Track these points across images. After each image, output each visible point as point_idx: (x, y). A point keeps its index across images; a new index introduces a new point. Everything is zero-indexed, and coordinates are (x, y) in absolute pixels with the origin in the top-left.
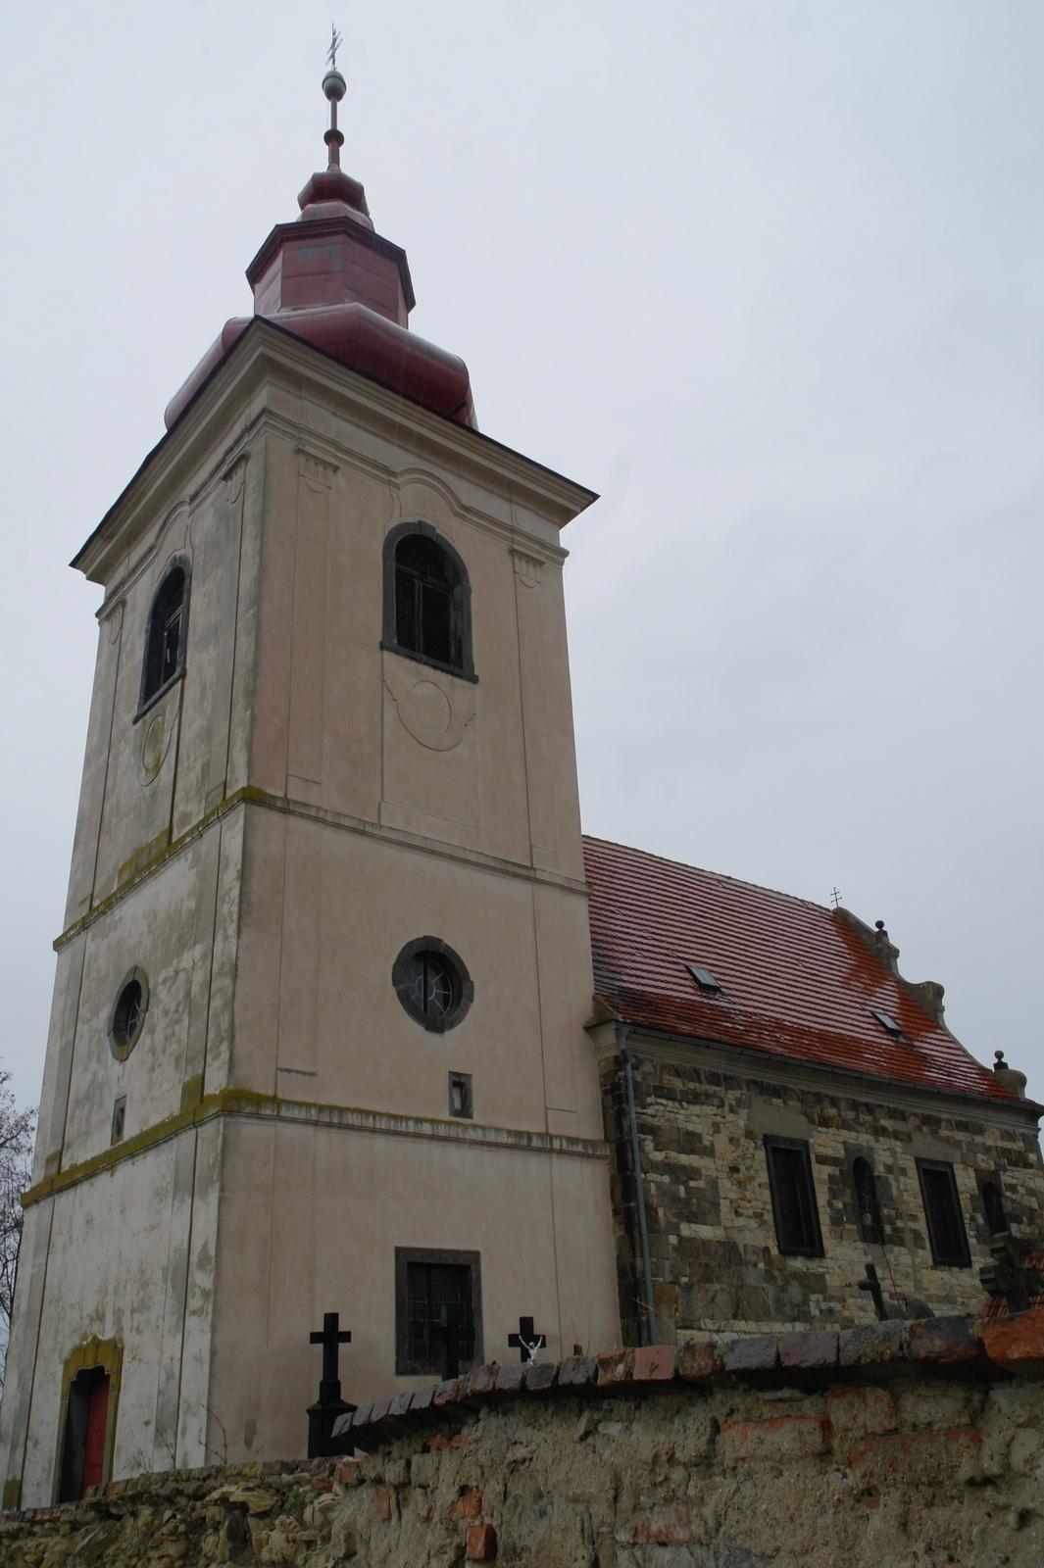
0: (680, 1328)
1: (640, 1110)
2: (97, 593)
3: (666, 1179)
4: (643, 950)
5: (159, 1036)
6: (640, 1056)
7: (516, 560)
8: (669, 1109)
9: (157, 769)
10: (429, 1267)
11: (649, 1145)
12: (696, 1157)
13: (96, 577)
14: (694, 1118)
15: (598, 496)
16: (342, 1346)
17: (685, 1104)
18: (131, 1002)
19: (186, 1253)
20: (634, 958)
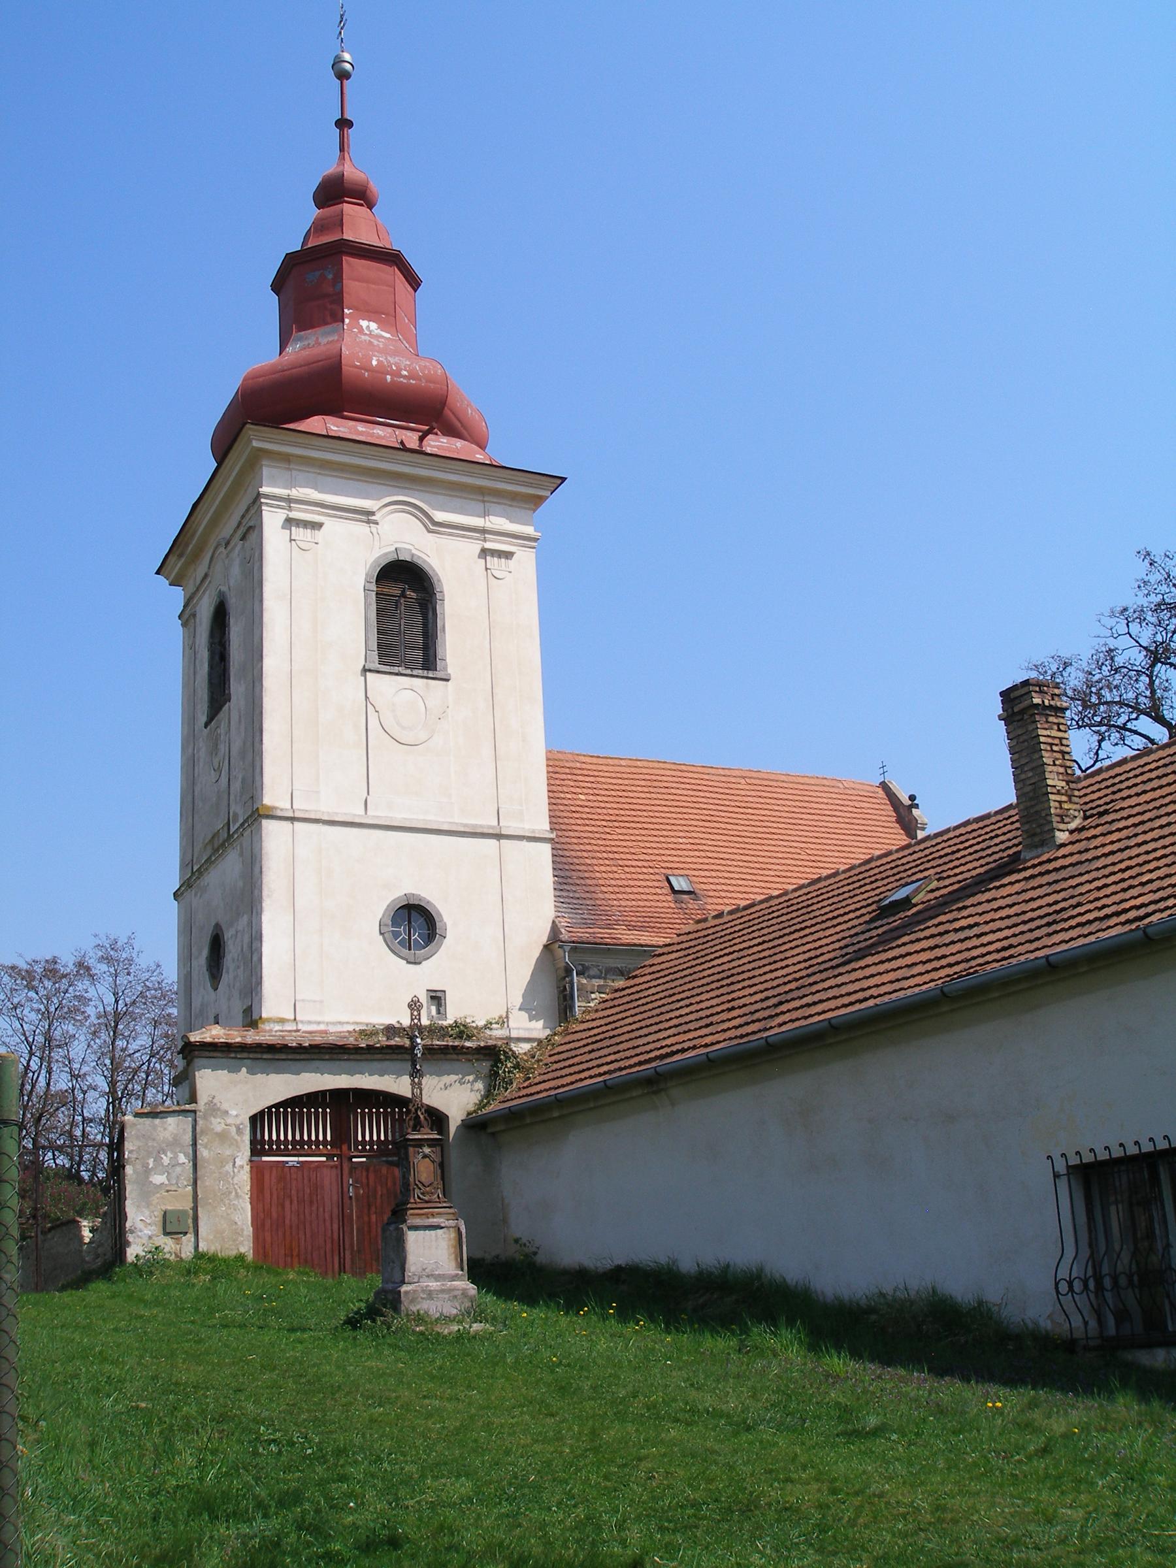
2: (177, 596)
5: (231, 976)
7: (488, 558)
9: (218, 770)
18: (217, 945)
20: (617, 876)
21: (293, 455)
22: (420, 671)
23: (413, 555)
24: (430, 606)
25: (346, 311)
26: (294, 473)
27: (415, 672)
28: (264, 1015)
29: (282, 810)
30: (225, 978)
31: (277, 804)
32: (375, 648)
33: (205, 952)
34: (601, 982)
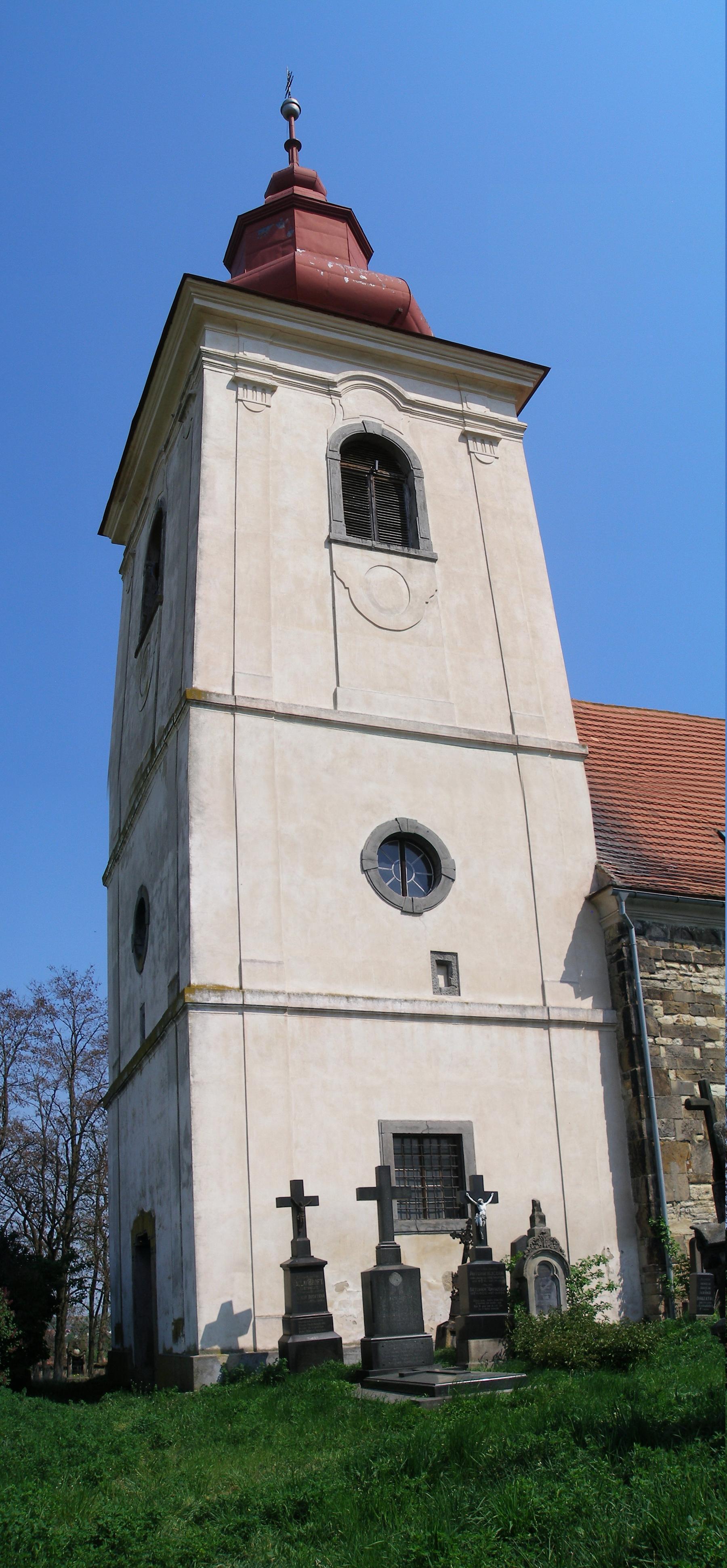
0: (692, 1183)
1: (647, 975)
3: (679, 1042)
4: (668, 818)
6: (647, 921)
8: (681, 972)
10: (421, 1137)
11: (658, 1008)
12: (714, 1018)
13: (115, 541)
14: (711, 980)
15: (549, 369)
16: (309, 1210)
17: (700, 967)
19: (177, 1133)
21: (241, 319)
22: (399, 548)
23: (383, 430)
24: (406, 487)
25: (298, 250)
26: (242, 339)
27: (393, 548)
28: (194, 981)
29: (218, 695)
30: (152, 950)
31: (213, 689)
32: (342, 518)
33: (131, 931)
34: (667, 946)
